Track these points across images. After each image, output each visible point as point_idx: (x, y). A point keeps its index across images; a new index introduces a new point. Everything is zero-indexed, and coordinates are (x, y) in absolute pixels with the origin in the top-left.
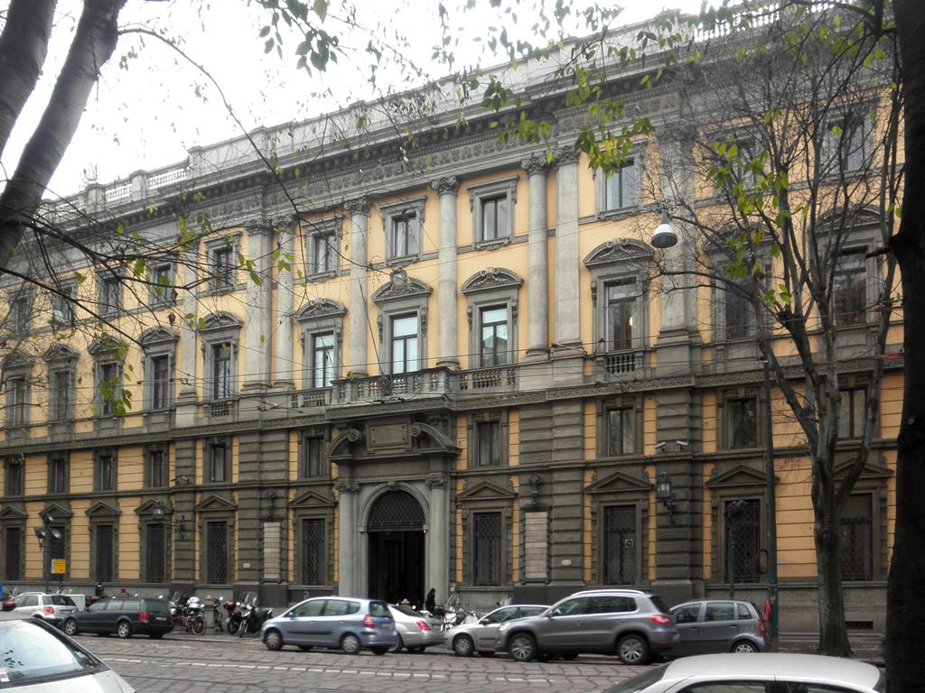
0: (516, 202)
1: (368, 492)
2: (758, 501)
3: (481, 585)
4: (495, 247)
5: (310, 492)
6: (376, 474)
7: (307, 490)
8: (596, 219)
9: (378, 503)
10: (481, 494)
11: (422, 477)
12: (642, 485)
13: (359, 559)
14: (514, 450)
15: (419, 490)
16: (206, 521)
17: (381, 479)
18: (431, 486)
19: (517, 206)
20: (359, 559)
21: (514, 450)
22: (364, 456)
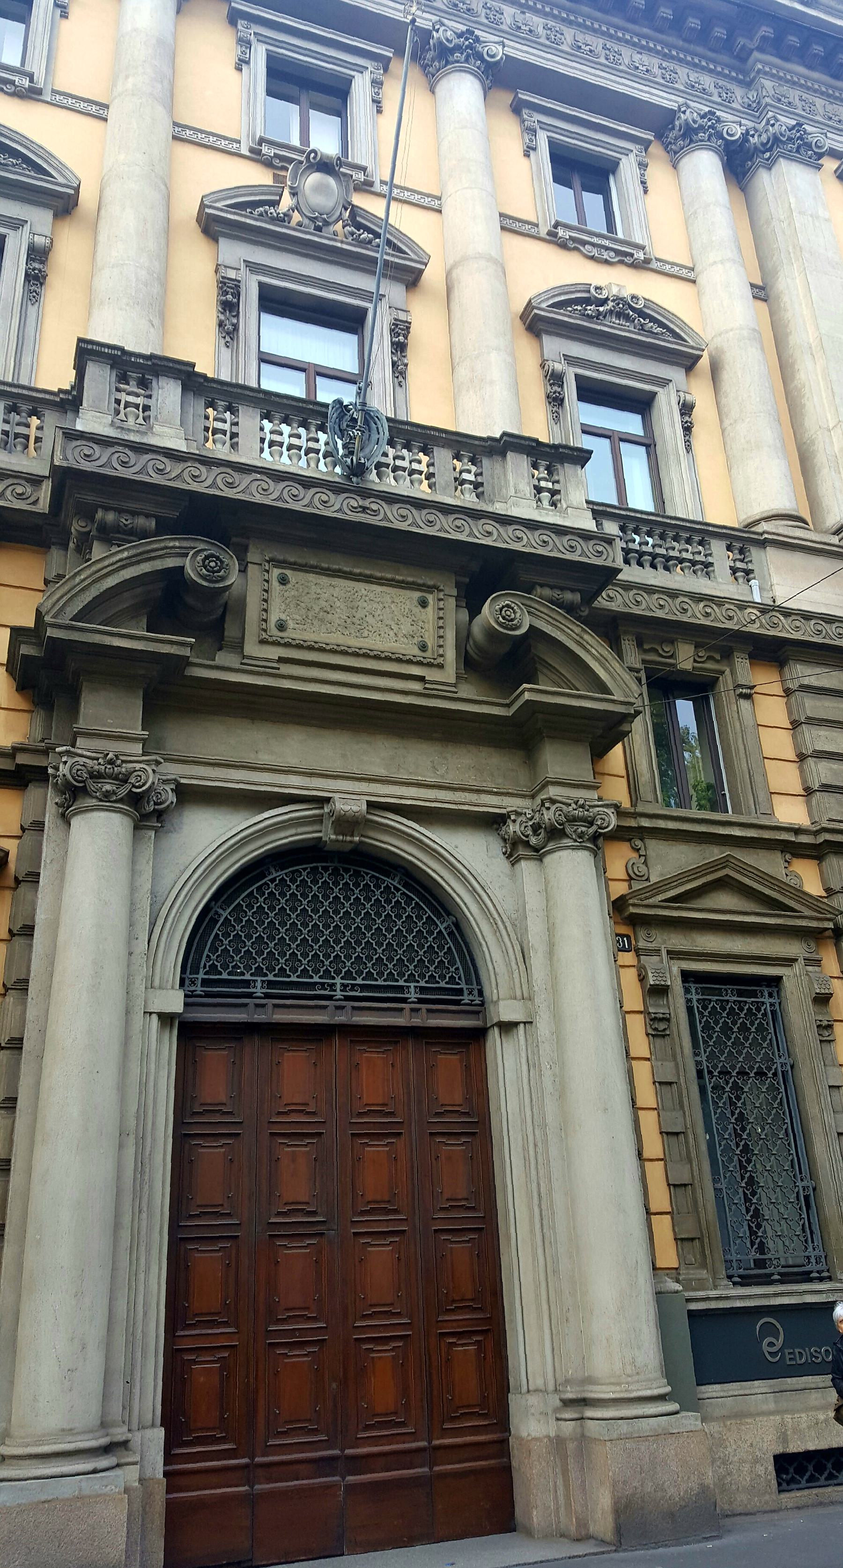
0: (65, 16)
1: (207, 839)
2: (776, 981)
3: (786, 1278)
4: (606, 255)
5: (724, 863)
6: (265, 758)
7: (716, 853)
8: (543, 231)
9: (243, 884)
10: (709, 901)
11: (490, 804)
12: (807, 912)
13: (142, 1165)
14: (784, 777)
15: (469, 861)
16: (676, 967)
17: (294, 784)
18: (526, 847)
19: (65, 26)
20: (142, 1165)
21: (784, 777)
22: (223, 669)
